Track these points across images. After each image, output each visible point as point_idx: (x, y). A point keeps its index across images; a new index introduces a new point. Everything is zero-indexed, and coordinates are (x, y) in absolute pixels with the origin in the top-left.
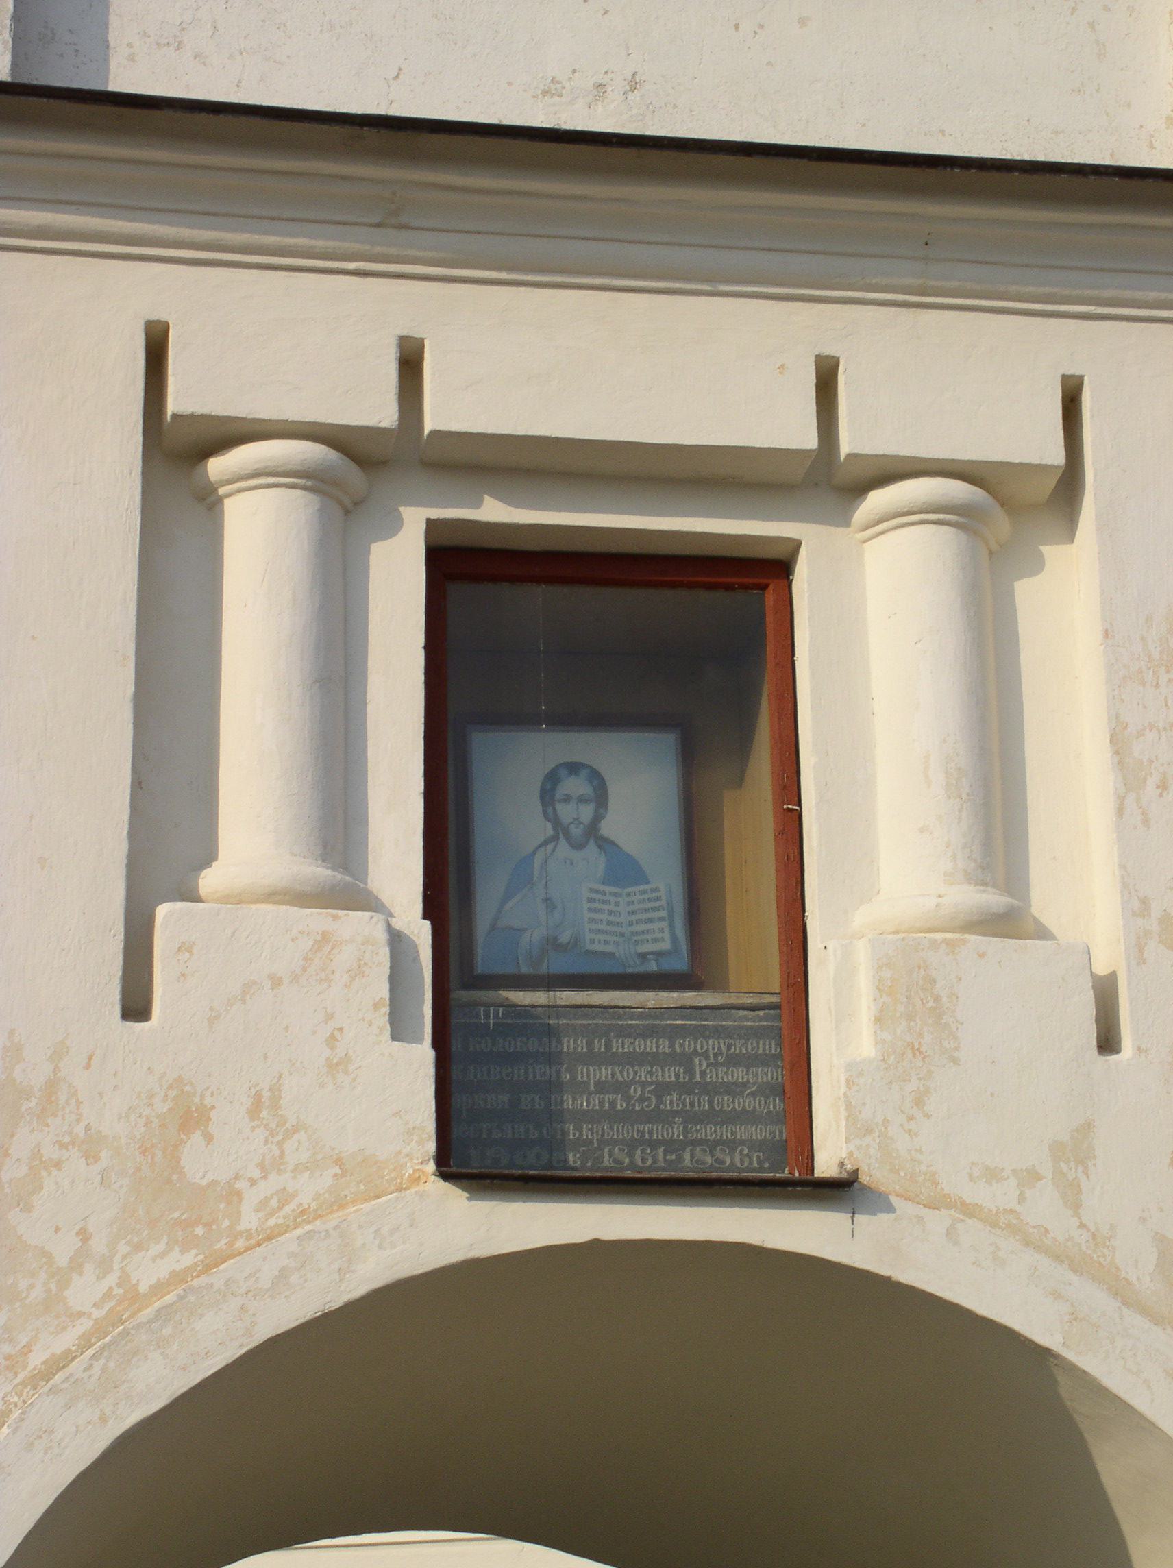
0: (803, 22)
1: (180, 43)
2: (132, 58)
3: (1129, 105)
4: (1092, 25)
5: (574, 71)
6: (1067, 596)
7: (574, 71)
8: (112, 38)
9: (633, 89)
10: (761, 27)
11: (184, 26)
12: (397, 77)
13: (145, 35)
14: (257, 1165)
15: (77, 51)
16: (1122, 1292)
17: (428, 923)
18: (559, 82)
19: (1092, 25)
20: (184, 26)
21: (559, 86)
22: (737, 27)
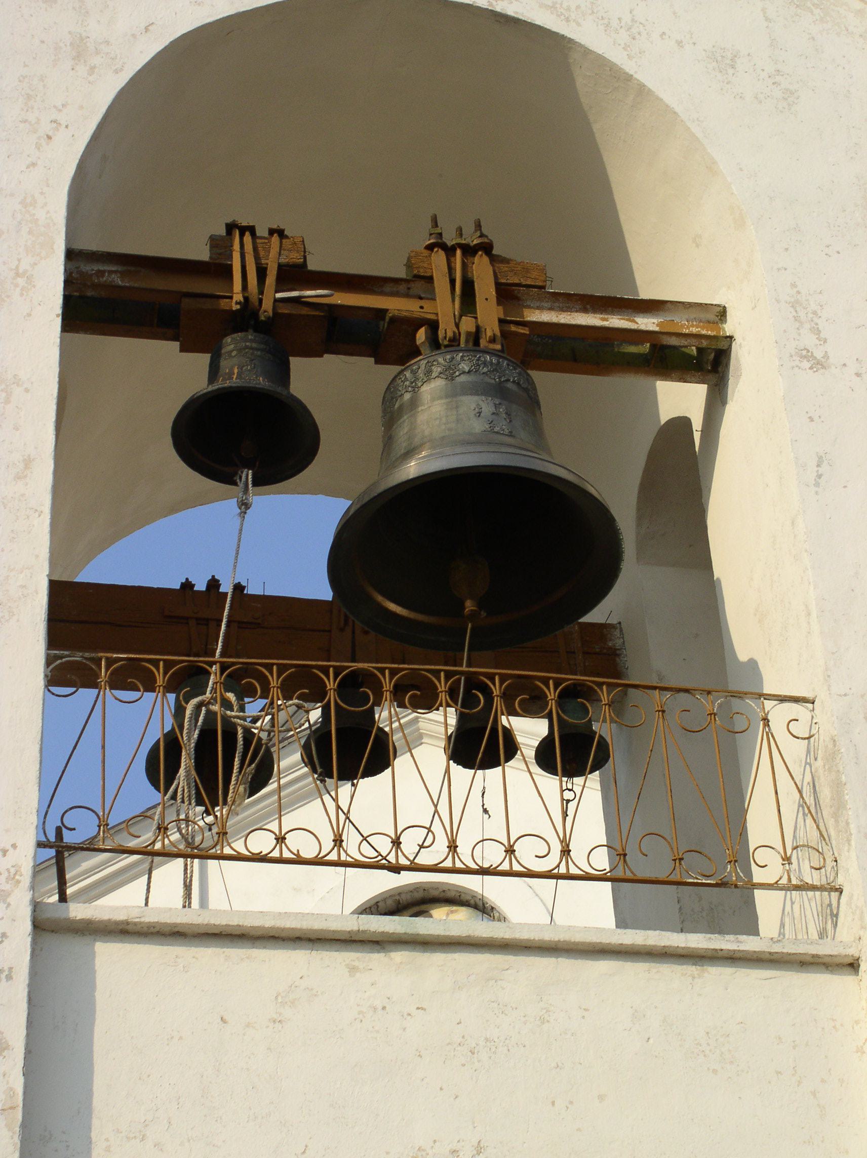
0: (601, 1098)
1: (144, 1136)
2: (108, 1149)
3: (847, 1152)
4: (814, 1094)
5: (435, 1141)
6: (683, 862)
7: (435, 1141)
8: (93, 1135)
9: (479, 1153)
10: (571, 1103)
11: (147, 1123)
12: (304, 1152)
13: (118, 1131)
14: (20, 203)
15: (68, 1146)
16: (519, 285)
17: (177, 586)
18: (423, 1150)
19: (814, 1094)
20: (147, 1123)
21: (424, 1153)
22: (553, 1103)
